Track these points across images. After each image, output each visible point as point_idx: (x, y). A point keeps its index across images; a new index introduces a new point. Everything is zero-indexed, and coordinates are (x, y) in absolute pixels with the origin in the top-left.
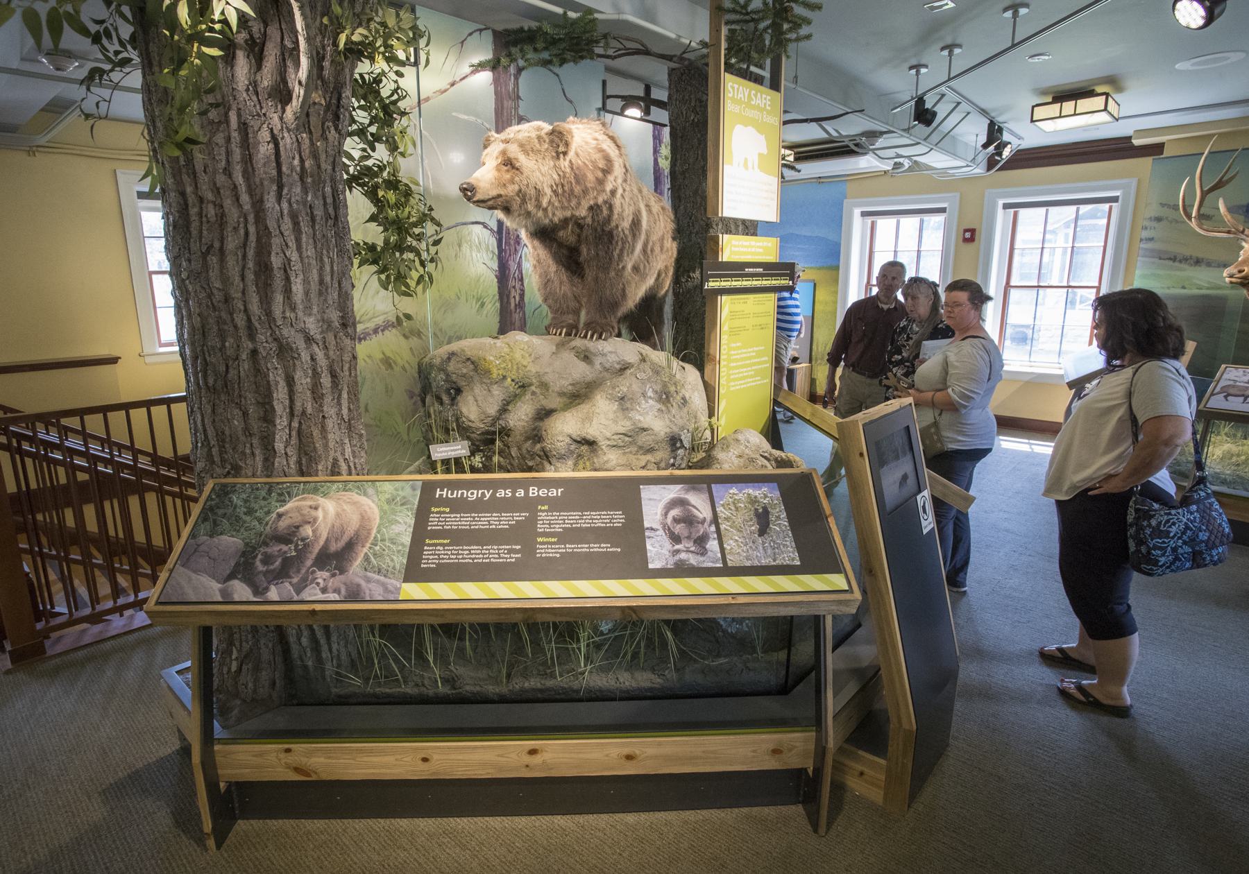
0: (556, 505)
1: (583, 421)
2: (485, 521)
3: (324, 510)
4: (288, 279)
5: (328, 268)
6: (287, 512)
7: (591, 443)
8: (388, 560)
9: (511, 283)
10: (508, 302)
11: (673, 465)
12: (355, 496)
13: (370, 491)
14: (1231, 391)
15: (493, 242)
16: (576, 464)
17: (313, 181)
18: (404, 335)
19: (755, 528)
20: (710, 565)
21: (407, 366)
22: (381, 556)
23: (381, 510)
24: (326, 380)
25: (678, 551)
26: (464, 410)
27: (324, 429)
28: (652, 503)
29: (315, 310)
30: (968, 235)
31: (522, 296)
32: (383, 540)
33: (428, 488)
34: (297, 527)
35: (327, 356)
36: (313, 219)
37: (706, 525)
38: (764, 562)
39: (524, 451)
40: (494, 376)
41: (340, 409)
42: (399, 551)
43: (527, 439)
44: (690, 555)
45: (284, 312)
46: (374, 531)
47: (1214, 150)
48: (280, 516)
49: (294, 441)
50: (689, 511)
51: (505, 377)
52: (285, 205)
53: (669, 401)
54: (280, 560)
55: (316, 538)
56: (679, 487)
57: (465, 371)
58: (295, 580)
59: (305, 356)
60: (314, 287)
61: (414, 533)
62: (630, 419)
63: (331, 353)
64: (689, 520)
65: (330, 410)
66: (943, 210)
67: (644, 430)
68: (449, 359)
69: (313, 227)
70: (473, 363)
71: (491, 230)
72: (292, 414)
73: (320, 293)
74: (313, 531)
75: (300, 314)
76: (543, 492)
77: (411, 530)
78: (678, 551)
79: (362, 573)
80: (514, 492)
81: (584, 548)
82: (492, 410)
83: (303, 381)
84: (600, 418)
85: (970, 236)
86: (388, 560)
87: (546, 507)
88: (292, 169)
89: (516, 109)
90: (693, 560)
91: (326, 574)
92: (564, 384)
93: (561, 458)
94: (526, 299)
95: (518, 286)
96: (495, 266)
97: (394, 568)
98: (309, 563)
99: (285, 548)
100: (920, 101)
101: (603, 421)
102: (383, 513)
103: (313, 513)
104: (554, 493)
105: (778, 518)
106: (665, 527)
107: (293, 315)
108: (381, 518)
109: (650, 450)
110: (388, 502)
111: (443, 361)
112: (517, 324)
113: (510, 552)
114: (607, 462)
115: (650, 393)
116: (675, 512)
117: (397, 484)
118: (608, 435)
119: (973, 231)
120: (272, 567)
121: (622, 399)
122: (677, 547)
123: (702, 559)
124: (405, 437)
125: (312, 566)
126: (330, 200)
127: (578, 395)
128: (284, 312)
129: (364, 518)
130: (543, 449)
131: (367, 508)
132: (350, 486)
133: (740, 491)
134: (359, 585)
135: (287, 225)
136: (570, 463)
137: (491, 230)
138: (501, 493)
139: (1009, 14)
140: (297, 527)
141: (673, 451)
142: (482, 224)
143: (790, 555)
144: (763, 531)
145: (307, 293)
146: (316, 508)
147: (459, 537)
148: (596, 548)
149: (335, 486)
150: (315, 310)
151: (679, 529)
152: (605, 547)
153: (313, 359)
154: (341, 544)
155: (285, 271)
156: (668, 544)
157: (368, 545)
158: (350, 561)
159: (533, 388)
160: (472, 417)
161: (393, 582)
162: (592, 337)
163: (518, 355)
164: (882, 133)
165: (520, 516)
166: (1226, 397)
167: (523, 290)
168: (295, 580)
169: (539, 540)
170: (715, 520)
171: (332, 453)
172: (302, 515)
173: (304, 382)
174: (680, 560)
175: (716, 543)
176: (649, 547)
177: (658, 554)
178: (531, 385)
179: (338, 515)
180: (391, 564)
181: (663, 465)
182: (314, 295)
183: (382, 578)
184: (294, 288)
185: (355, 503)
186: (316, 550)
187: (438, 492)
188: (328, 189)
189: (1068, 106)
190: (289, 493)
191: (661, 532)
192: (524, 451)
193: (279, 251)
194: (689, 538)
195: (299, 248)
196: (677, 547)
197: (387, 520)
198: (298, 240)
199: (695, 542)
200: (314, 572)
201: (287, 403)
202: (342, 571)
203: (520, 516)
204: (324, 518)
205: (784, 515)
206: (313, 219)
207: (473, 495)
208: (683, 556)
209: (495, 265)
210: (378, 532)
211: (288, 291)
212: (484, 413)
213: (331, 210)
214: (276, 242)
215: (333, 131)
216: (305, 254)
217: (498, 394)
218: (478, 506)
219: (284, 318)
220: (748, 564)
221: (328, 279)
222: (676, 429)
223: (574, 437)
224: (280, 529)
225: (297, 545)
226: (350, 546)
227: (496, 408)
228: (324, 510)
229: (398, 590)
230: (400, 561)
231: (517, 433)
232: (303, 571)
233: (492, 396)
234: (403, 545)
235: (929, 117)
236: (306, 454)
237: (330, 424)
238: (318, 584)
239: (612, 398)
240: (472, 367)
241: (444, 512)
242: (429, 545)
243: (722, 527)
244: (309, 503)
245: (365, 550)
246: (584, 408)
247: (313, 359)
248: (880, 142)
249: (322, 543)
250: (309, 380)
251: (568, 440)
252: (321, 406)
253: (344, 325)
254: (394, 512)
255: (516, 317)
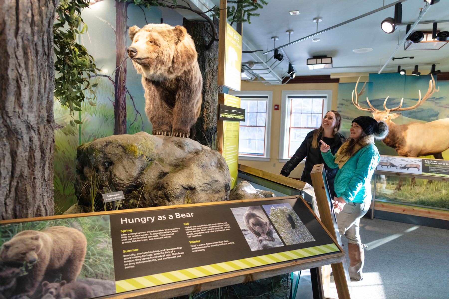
0: (192, 222)
1: (188, 177)
2: (157, 235)
3: (43, 239)
4: (19, 87)
5: (43, 84)
6: (13, 244)
7: (192, 189)
8: (101, 268)
9: (121, 110)
10: (119, 120)
11: (226, 199)
12: (65, 228)
13: (75, 224)
14: (383, 164)
15: (113, 88)
16: (184, 201)
17: (38, 30)
18: (65, 133)
19: (289, 225)
20: (278, 246)
21: (66, 152)
22: (95, 265)
23: (86, 235)
24: (38, 155)
25: (261, 241)
26: (117, 174)
27: (34, 187)
28: (239, 216)
29: (35, 109)
30: (276, 107)
31: (125, 117)
32: (94, 255)
33: (114, 219)
34: (25, 254)
35: (39, 139)
36: (37, 53)
37: (268, 225)
38: (301, 241)
39: (153, 195)
40: (137, 154)
41: (44, 173)
42: (107, 261)
43: (155, 188)
44: (268, 242)
45: (14, 108)
46: (85, 250)
47: (361, 82)
48: (7, 247)
49: (13, 195)
50: (258, 220)
51: (142, 155)
52: (20, 40)
53: (222, 167)
54: (15, 280)
55: (42, 259)
56: (248, 208)
57: (117, 152)
58: (32, 293)
59: (26, 138)
60: (35, 95)
61: (114, 247)
62: (210, 176)
63: (42, 137)
64: (259, 223)
65: (38, 174)
66: (267, 97)
67: (216, 181)
68: (107, 145)
69: (37, 57)
70: (123, 147)
71: (112, 81)
72: (12, 177)
73: (38, 99)
74: (39, 255)
75: (25, 110)
76: (183, 216)
77: (111, 245)
78: (261, 241)
79: (84, 279)
80: (167, 217)
81: (215, 244)
82: (135, 173)
83: (23, 154)
84: (196, 176)
85: (277, 107)
86: (101, 268)
87: (188, 224)
88: (26, 18)
89: (126, 22)
90: (270, 244)
91: (56, 285)
92: (172, 159)
93: (177, 197)
94: (127, 118)
95: (123, 112)
96: (114, 101)
97: (106, 272)
98: (40, 278)
99: (17, 270)
100: (276, 51)
101: (198, 177)
102: (89, 238)
103: (35, 242)
104: (189, 215)
105: (296, 219)
106: (250, 228)
107: (20, 111)
108: (88, 240)
109: (218, 192)
110: (90, 229)
111: (102, 146)
112: (123, 131)
113: (177, 251)
114: (200, 198)
115: (213, 164)
116: (252, 221)
117: (93, 218)
118: (201, 184)
119: (278, 106)
120: (8, 287)
121: (203, 166)
122: (260, 238)
123: (274, 243)
124: (62, 193)
125: (44, 280)
126: (46, 44)
127: (180, 165)
128: (14, 108)
129: (75, 242)
130: (165, 194)
131: (76, 235)
132: (59, 221)
133: (276, 207)
134: (84, 288)
135: (20, 53)
136: (181, 200)
137: (112, 81)
138: (160, 218)
139: (315, 21)
140: (25, 254)
141: (226, 192)
142: (109, 77)
143: (310, 238)
144: (293, 226)
145: (30, 98)
146: (37, 239)
147: (144, 246)
148: (222, 243)
149: (48, 223)
150: (35, 109)
151: (257, 228)
152: (225, 243)
153: (31, 140)
154: (63, 261)
155: (17, 81)
156: (255, 237)
157: (83, 259)
158: (73, 272)
159: (155, 161)
160: (122, 178)
161: (109, 282)
162: (182, 136)
163: (149, 143)
164: (256, 63)
165: (176, 230)
166: (382, 166)
167: (126, 114)
168: (32, 293)
169: (191, 242)
170: (271, 223)
171: (37, 203)
172: (26, 245)
173: (23, 155)
174: (265, 245)
175: (276, 234)
176: (247, 240)
177: (253, 243)
178: (155, 160)
179: (55, 242)
180: (103, 269)
181: (223, 199)
182: (35, 100)
183: (100, 281)
184: (23, 94)
185: (66, 233)
186: (44, 268)
187: (122, 221)
188: (45, 37)
189: (319, 60)
190: (11, 231)
191: (249, 231)
192: (153, 195)
193: (14, 68)
194: (263, 233)
195: (27, 68)
196: (260, 238)
197: (92, 241)
198: (26, 64)
199: (267, 235)
200: (45, 285)
201: (10, 168)
202: (69, 280)
203: (176, 230)
204: (45, 245)
205: (298, 218)
206: (37, 53)
207: (144, 220)
208: (265, 242)
209: (113, 99)
210: (89, 249)
211: (18, 95)
212: (130, 175)
213: (46, 50)
214: (12, 62)
215: (51, 3)
216: (30, 73)
217: (138, 164)
218: (149, 227)
219: (14, 112)
220: (294, 243)
221: (43, 91)
222: (227, 181)
223: (184, 186)
224: (10, 257)
225: (27, 267)
226: (70, 262)
227: (137, 172)
228: (43, 239)
229: (114, 286)
230: (110, 266)
231: (149, 185)
232: (37, 285)
233: (135, 165)
234: (108, 256)
235: (281, 57)
236: (20, 203)
237: (38, 182)
238: (51, 293)
239: (198, 166)
240: (122, 149)
241: (130, 232)
242: (126, 254)
243: (276, 226)
244: (30, 236)
245: (82, 263)
246: (186, 172)
247: (31, 140)
248: (254, 67)
249: (47, 262)
250: (27, 154)
251: (181, 188)
252: (33, 171)
253: (49, 122)
254: (96, 236)
255: (122, 127)
